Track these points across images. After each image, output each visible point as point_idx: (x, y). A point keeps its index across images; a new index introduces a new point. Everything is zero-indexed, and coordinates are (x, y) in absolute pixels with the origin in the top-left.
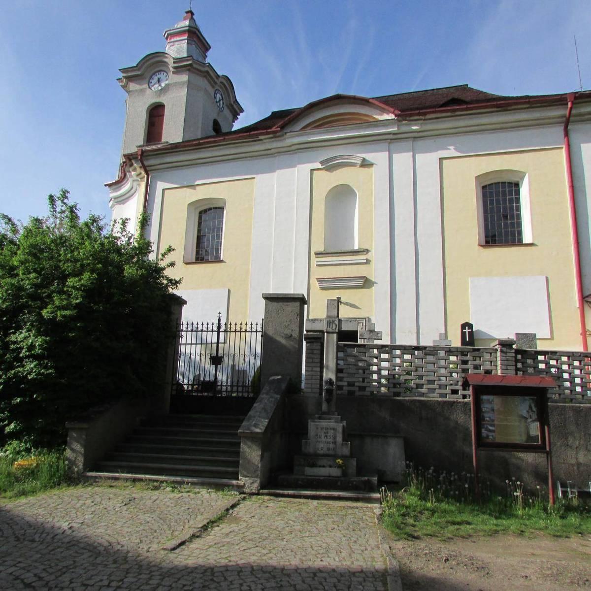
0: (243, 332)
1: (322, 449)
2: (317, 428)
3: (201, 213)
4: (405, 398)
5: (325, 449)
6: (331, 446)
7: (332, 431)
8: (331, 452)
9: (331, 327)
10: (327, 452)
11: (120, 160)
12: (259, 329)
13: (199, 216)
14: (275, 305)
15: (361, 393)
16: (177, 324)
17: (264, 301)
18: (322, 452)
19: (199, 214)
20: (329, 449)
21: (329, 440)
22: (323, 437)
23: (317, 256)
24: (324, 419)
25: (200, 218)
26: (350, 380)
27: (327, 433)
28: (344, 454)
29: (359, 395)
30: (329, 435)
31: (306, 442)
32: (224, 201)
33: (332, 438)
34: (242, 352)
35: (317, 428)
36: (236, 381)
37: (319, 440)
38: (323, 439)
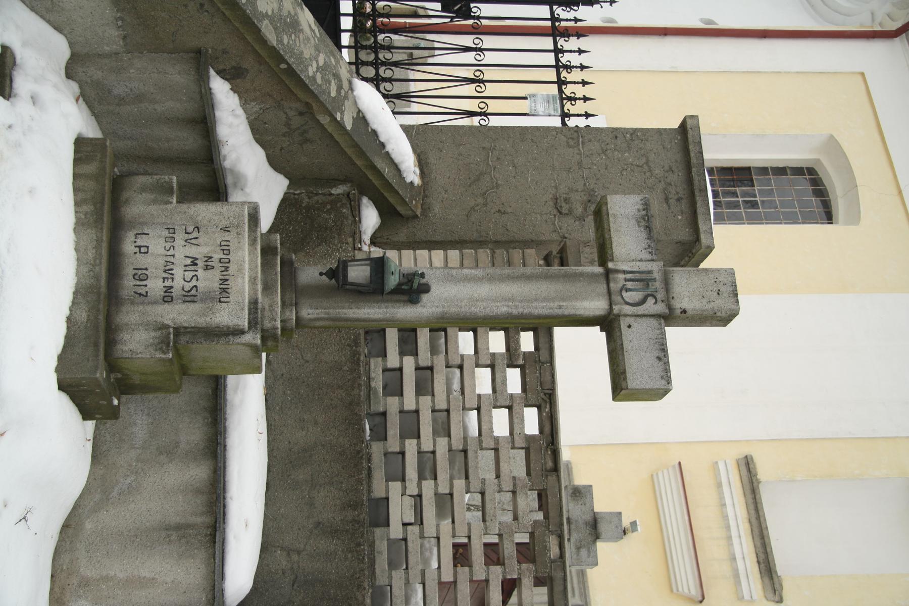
0: (558, 74)
1: (143, 250)
2: (226, 229)
3: (811, 171)
4: (362, 366)
5: (143, 261)
6: (155, 286)
7: (216, 286)
8: (128, 284)
9: (629, 285)
10: (129, 271)
11: (862, 71)
12: (572, 122)
13: (802, 169)
14: (674, 156)
15: (378, 383)
16: (490, 319)
17: (675, 124)
18: (128, 246)
19: (808, 169)
20: (141, 276)
21: (178, 272)
22: (193, 251)
23: (743, 463)
24: (267, 265)
25: (798, 171)
26: (426, 419)
27: (207, 268)
28: (125, 336)
29: (372, 545)
30: (201, 273)
31: (170, 191)
32: (855, 218)
33: (188, 286)
34: (489, 74)
35: (226, 229)
36: (394, 60)
37: (180, 237)
38: (182, 252)
